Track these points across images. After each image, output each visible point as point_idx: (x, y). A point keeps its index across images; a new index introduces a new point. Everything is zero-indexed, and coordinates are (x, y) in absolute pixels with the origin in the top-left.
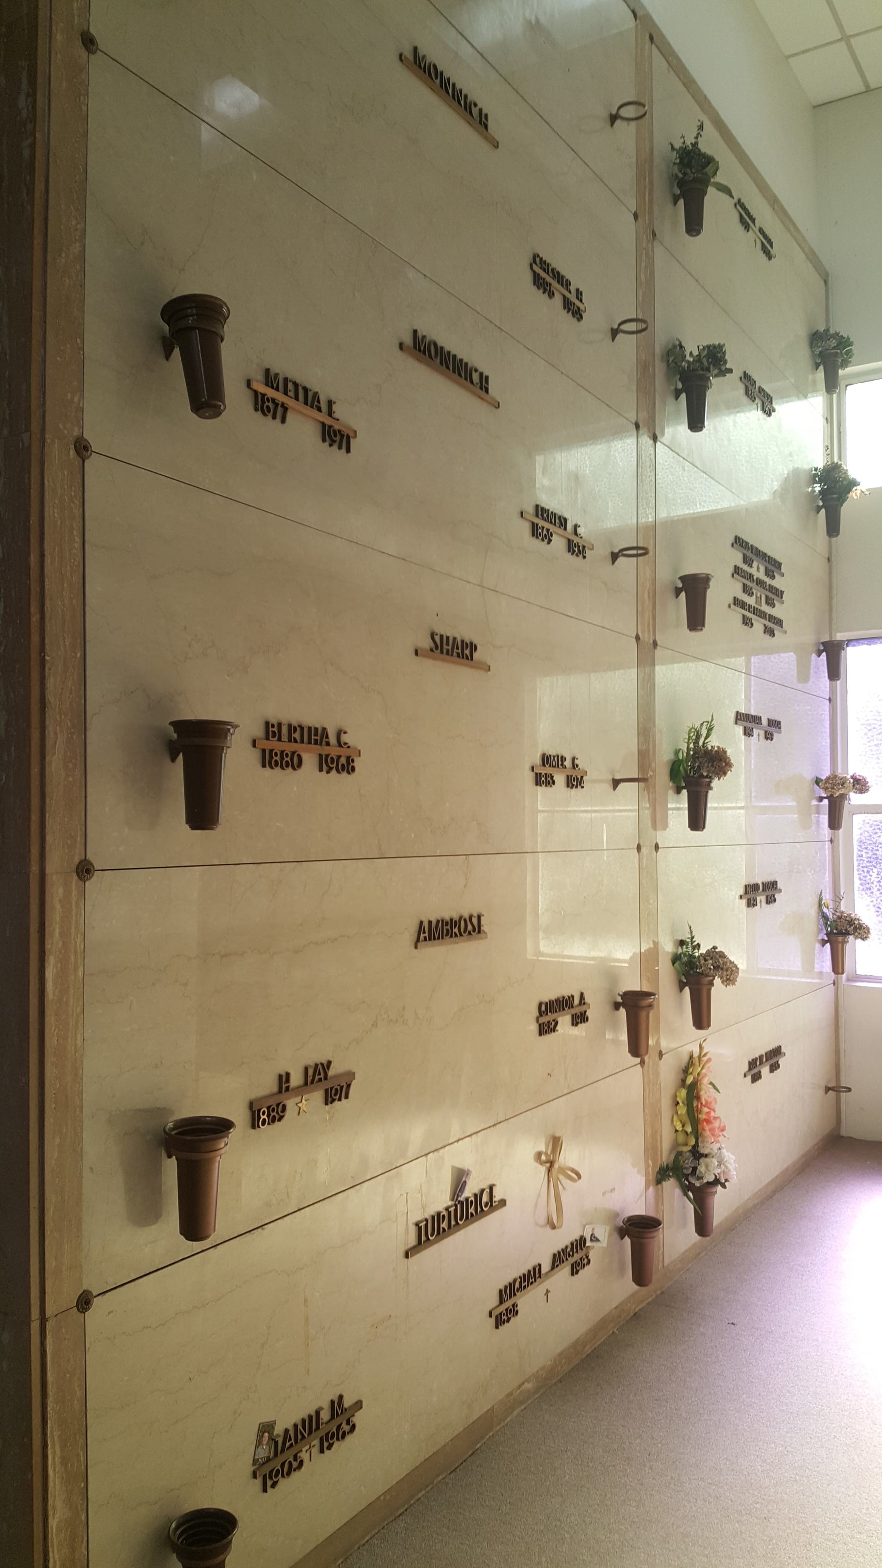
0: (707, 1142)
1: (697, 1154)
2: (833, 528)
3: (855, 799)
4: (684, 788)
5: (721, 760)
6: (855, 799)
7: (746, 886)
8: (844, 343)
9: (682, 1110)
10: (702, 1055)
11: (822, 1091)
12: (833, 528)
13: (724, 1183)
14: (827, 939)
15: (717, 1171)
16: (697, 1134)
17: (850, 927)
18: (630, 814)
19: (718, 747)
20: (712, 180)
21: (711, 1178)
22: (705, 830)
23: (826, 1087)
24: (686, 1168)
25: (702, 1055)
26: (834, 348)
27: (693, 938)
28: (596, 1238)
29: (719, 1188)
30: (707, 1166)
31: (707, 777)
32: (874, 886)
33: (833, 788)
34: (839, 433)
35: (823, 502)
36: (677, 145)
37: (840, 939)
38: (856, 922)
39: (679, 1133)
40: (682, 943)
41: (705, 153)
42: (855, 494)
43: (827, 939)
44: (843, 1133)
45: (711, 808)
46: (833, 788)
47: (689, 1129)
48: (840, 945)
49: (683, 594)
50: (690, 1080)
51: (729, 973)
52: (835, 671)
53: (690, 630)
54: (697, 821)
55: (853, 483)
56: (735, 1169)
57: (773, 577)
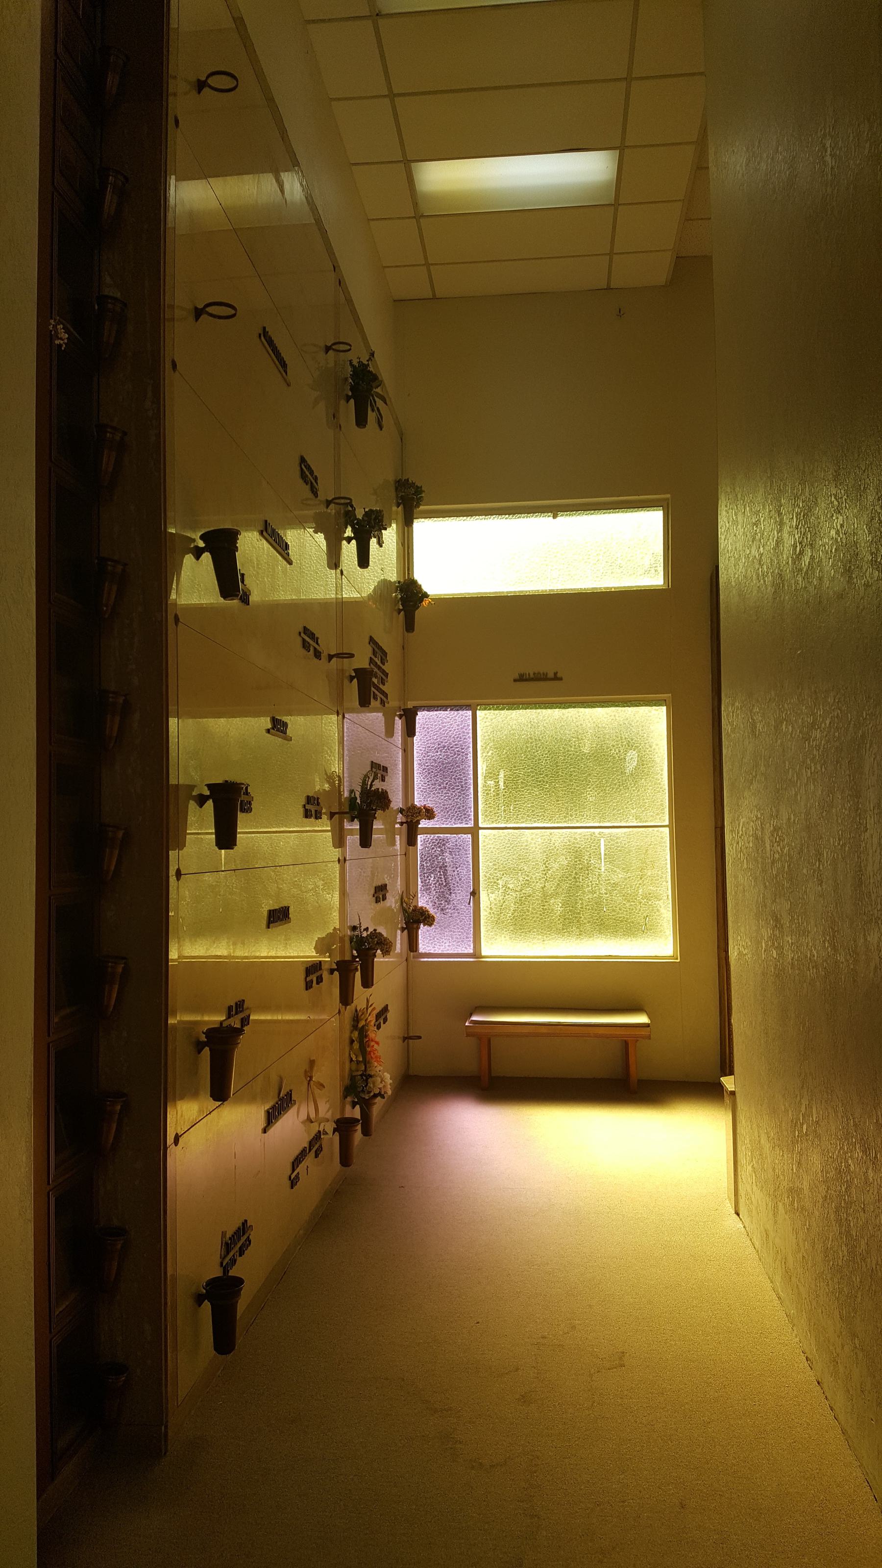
0: (373, 1066)
1: (367, 1077)
2: (410, 625)
3: (424, 824)
4: (355, 817)
5: (385, 799)
6: (424, 824)
7: (375, 887)
8: (419, 490)
9: (356, 1045)
10: (370, 1005)
11: (401, 1041)
12: (410, 625)
13: (383, 1095)
14: (405, 926)
15: (381, 1086)
16: (366, 1062)
17: (422, 917)
18: (209, 836)
19: (382, 789)
20: (374, 390)
21: (377, 1091)
22: (371, 848)
23: (404, 1037)
24: (359, 1087)
25: (370, 1005)
26: (413, 494)
27: (360, 924)
28: (326, 1132)
29: (379, 1098)
30: (374, 1083)
31: (374, 810)
32: (431, 887)
33: (413, 816)
34: (408, 553)
35: (403, 606)
36: (355, 363)
37: (415, 926)
38: (427, 913)
39: (353, 1062)
40: (354, 928)
41: (555, 517)
42: (425, 603)
43: (405, 926)
44: (411, 1072)
45: (240, 833)
46: (413, 816)
47: (361, 1059)
48: (415, 930)
49: (355, 680)
50: (360, 1025)
51: (388, 946)
52: (410, 730)
53: (361, 707)
54: (365, 841)
55: (426, 595)
56: (390, 1084)
57: (384, 664)
